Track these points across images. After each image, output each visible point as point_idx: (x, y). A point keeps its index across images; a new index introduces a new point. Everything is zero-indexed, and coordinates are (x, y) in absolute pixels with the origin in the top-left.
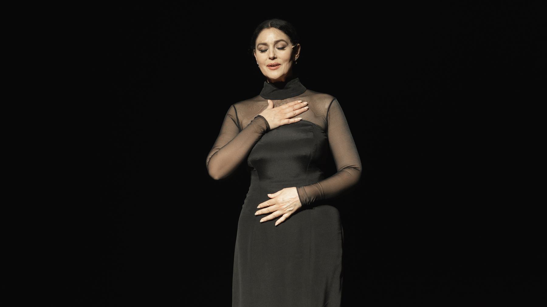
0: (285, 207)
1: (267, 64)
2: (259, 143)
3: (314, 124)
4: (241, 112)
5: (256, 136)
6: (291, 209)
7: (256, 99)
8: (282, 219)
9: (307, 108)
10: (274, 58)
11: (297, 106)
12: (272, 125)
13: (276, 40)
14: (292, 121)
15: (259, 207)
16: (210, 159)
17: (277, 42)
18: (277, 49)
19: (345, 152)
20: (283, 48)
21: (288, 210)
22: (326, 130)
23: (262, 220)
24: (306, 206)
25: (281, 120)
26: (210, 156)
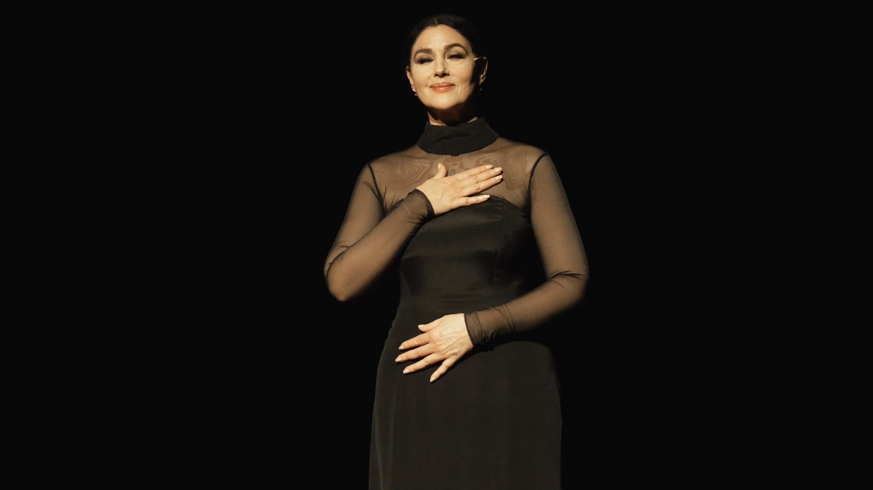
0: (443, 347)
1: (430, 84)
2: (421, 231)
3: (508, 202)
4: (385, 174)
5: (408, 228)
6: (456, 351)
7: (409, 152)
8: (442, 369)
9: (501, 177)
10: (444, 75)
11: (484, 176)
12: (438, 208)
13: (448, 44)
14: (473, 200)
15: (401, 347)
16: (331, 264)
17: (449, 48)
18: (448, 61)
19: (560, 243)
20: (459, 56)
21: (450, 352)
22: (527, 209)
23: (407, 370)
24: (482, 344)
25: (453, 199)
26: (330, 260)
